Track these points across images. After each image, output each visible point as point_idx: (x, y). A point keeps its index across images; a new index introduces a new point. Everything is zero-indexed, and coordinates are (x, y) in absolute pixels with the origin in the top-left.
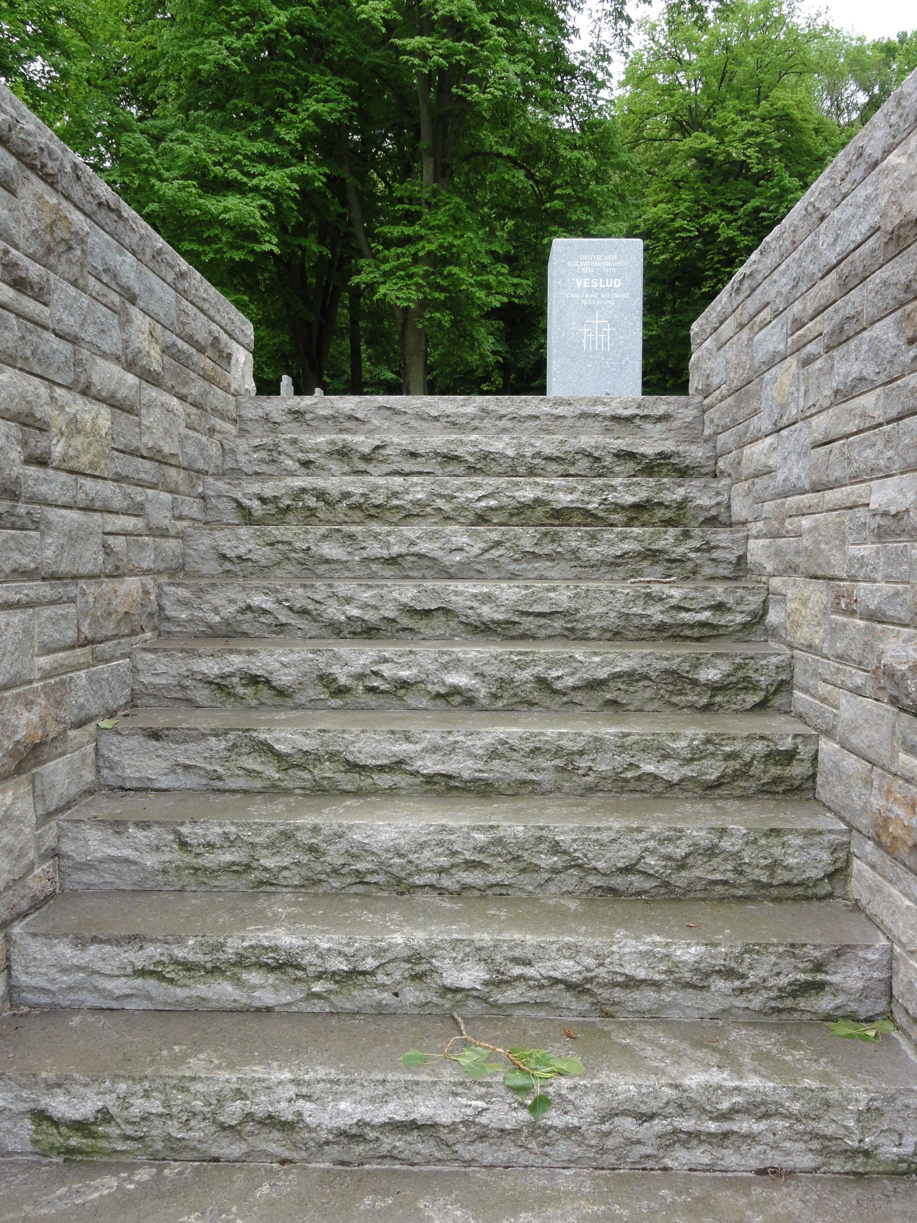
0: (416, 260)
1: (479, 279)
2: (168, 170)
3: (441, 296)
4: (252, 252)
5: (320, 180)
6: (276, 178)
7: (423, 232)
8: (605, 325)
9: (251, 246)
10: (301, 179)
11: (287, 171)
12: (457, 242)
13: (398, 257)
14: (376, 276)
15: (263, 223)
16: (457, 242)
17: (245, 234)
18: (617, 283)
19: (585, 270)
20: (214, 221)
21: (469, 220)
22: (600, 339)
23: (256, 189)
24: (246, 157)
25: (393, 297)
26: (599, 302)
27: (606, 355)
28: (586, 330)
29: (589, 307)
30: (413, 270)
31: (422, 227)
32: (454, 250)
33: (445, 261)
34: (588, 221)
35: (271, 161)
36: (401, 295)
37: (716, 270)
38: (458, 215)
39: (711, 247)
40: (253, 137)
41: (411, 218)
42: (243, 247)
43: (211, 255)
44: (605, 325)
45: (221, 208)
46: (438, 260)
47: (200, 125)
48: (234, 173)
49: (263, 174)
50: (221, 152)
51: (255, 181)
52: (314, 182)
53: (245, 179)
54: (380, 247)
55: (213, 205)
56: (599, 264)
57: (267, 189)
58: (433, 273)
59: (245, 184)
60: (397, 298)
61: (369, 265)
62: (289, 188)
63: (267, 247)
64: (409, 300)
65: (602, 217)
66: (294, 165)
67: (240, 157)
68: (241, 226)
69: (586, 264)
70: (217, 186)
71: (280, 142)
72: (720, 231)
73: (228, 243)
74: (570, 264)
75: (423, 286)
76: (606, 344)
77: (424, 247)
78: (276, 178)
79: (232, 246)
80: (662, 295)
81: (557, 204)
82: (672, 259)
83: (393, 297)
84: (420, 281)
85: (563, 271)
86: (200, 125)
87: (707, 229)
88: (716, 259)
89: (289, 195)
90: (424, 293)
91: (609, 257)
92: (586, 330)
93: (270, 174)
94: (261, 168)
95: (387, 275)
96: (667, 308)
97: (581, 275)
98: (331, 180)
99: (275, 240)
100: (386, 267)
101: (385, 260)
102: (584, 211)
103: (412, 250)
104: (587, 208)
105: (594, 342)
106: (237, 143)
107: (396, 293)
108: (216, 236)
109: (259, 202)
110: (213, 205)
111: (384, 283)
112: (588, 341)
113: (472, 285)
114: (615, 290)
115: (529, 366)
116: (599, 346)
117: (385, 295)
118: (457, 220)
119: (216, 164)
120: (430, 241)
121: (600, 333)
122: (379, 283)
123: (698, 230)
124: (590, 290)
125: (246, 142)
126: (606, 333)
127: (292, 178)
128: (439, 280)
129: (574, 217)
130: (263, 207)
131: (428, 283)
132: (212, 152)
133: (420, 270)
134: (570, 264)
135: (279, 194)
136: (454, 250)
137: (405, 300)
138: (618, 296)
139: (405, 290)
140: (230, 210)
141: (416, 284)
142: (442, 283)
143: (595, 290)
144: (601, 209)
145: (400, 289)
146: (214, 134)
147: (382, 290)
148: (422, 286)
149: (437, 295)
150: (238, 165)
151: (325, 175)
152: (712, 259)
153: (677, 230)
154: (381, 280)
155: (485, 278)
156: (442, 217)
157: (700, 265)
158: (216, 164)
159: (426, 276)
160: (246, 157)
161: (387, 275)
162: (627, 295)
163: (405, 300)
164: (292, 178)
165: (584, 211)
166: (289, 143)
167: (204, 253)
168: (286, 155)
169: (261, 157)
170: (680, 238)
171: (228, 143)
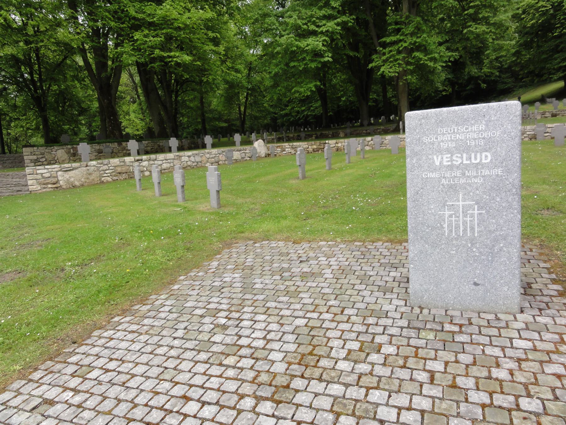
0: (399, 52)
1: (430, 56)
2: (285, 31)
3: (411, 68)
4: (320, 62)
5: (351, 22)
6: (331, 25)
7: (401, 38)
8: (471, 207)
9: (319, 59)
10: (344, 25)
11: (336, 21)
12: (418, 40)
13: (391, 51)
14: (380, 63)
15: (323, 48)
16: (418, 40)
17: (317, 54)
18: (487, 158)
19: (444, 146)
20: (303, 51)
21: (424, 28)
22: (465, 223)
23: (322, 33)
24: (317, 18)
25: (387, 72)
26: (462, 181)
27: (473, 241)
28: (447, 213)
29: (451, 187)
30: (397, 57)
31: (401, 35)
32: (417, 44)
33: (412, 50)
34: (488, 17)
35: (329, 18)
36: (391, 70)
37: (562, 23)
38: (419, 26)
39: (559, 12)
40: (320, 8)
41: (398, 31)
42: (316, 61)
43: (303, 66)
44: (471, 207)
45: (306, 45)
46: (409, 51)
47: (297, 8)
48: (312, 27)
49: (324, 25)
50: (306, 18)
51: (321, 29)
52: (348, 24)
53: (317, 29)
54: (381, 49)
55: (303, 44)
56: (462, 137)
57: (327, 31)
58: (407, 57)
59: (317, 31)
60: (389, 72)
61: (377, 58)
62: (336, 29)
63: (326, 59)
64: (395, 72)
65: (497, 11)
66: (339, 17)
67: (314, 19)
68: (315, 51)
69: (445, 138)
70: (304, 34)
71: (333, 8)
72: (564, 4)
73: (309, 60)
74: (425, 140)
75: (402, 64)
76: (472, 229)
77: (402, 45)
78: (331, 25)
79: (312, 61)
80: (532, 40)
81: (471, 11)
82: (537, 22)
83: (387, 72)
84: (400, 62)
85: (417, 149)
86: (297, 8)
87: (556, 4)
88: (562, 17)
89: (337, 33)
90: (403, 67)
91: (475, 128)
92: (447, 213)
93: (329, 24)
94: (324, 22)
95: (385, 61)
96: (535, 45)
97: (440, 152)
98: (357, 20)
99: (330, 55)
100: (384, 58)
101: (384, 54)
102: (486, 12)
103: (397, 47)
104: (488, 10)
105: (457, 227)
106: (313, 13)
107: (388, 70)
108: (305, 57)
109: (322, 39)
110: (303, 44)
111: (384, 65)
112: (450, 225)
113: (426, 60)
114: (483, 166)
115: (464, 82)
116: (465, 230)
117: (383, 72)
118: (419, 29)
119: (304, 24)
120: (405, 42)
121: (465, 216)
122: (382, 66)
123: (551, 5)
124: (451, 167)
125: (318, 11)
126: (472, 216)
127: (338, 24)
128: (410, 60)
129: (481, 16)
130: (324, 40)
131: (405, 62)
132: (303, 19)
133: (400, 57)
134: (425, 140)
135: (332, 33)
136: (417, 44)
137: (393, 72)
138: (487, 173)
139: (393, 68)
140: (309, 45)
141: (399, 64)
142: (411, 61)
143: (458, 167)
144: (497, 8)
145: (391, 68)
146: (303, 11)
147: (382, 70)
148: (401, 64)
149: (409, 67)
150: (314, 23)
151: (353, 19)
152: (559, 18)
153: (540, 7)
154: (382, 64)
155: (433, 55)
156: (411, 29)
157: (552, 21)
158: (304, 24)
159: (404, 58)
160: (317, 18)
161: (385, 61)
162: (499, 171)
163: (393, 72)
164: (338, 24)
165: (486, 12)
166: (336, 8)
167: (300, 66)
168: (335, 13)
169: (325, 17)
170: (541, 11)
171: (309, 14)
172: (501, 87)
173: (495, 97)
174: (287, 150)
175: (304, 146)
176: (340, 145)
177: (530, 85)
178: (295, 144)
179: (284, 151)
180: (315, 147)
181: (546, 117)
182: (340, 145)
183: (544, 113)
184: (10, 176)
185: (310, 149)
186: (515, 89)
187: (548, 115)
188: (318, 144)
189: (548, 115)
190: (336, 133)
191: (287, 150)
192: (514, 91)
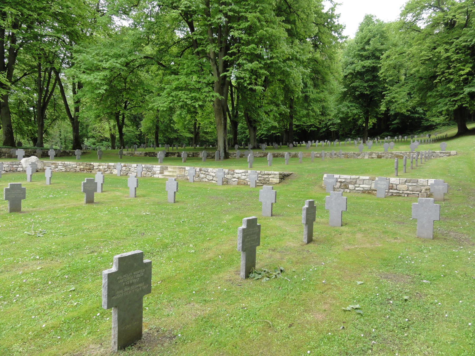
153: (422, 56)
172: (425, 124)
173: (420, 132)
174: (59, 167)
175: (74, 166)
176: (101, 167)
177: (453, 124)
178: (66, 163)
179: (57, 168)
180: (82, 167)
181: (373, 158)
182: (101, 167)
183: (371, 154)
184: (6, 163)
185: (78, 169)
186: (438, 127)
187: (374, 155)
188: (85, 165)
189: (374, 155)
190: (196, 153)
191: (59, 167)
192: (437, 128)
